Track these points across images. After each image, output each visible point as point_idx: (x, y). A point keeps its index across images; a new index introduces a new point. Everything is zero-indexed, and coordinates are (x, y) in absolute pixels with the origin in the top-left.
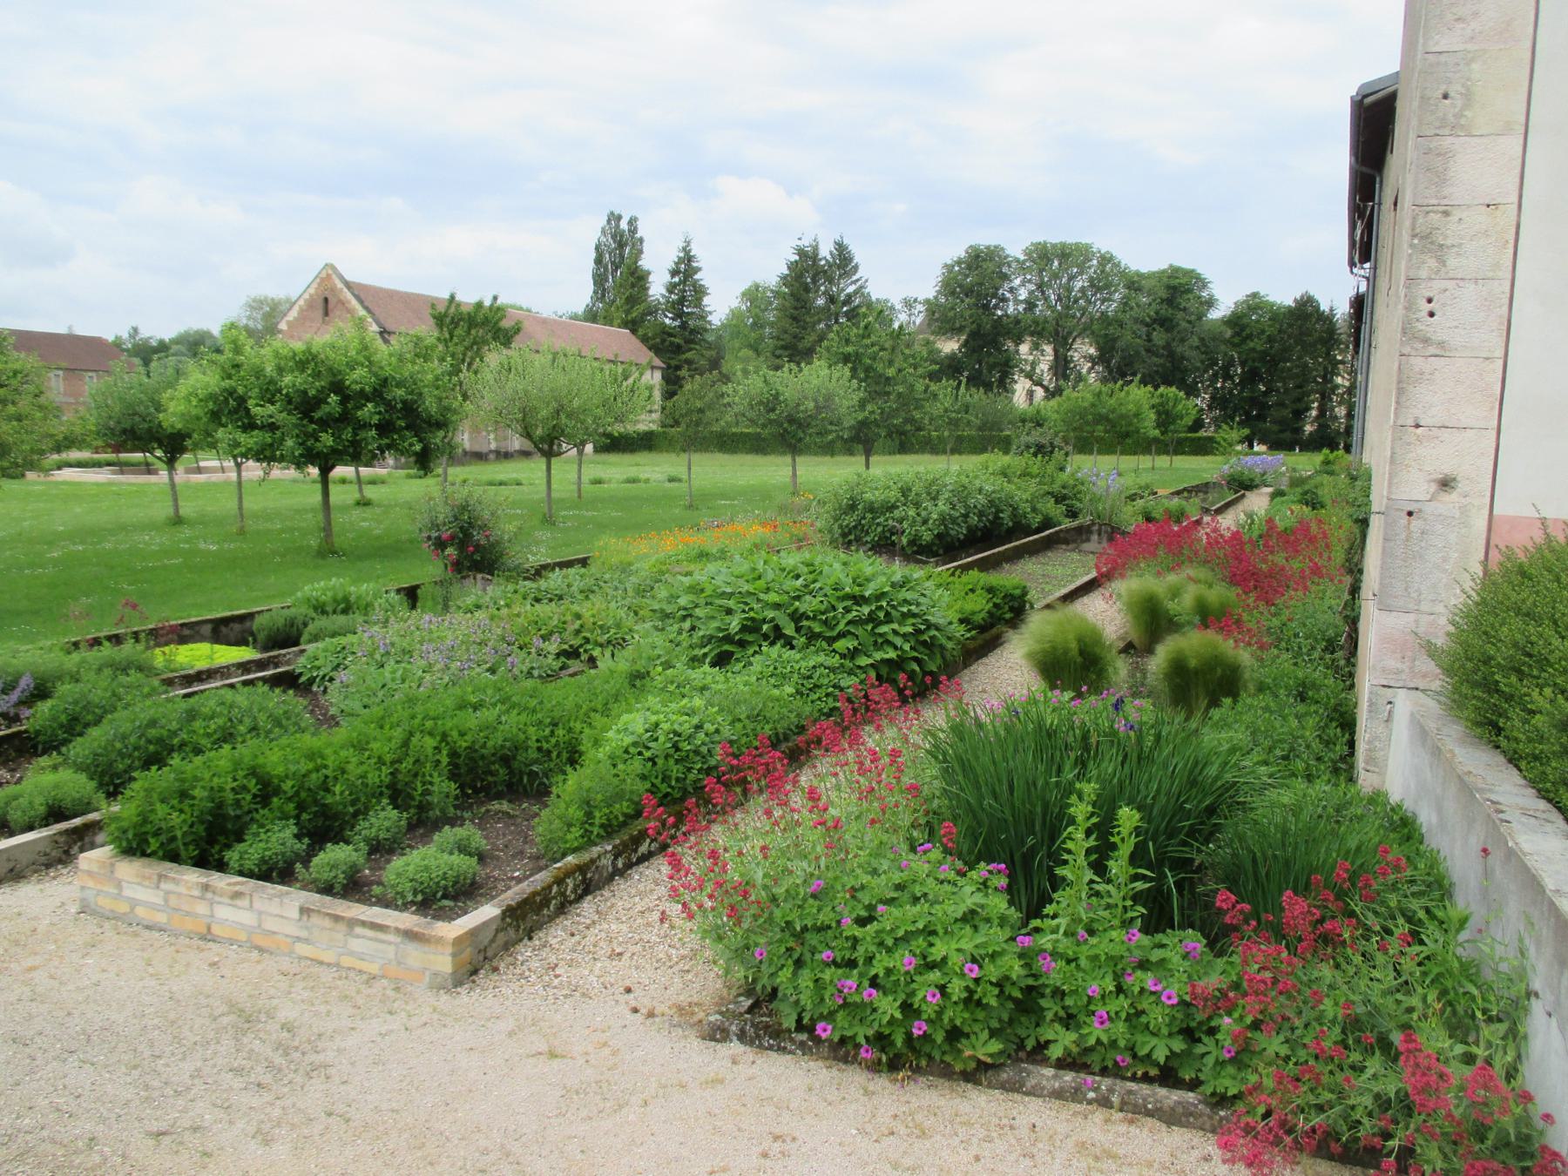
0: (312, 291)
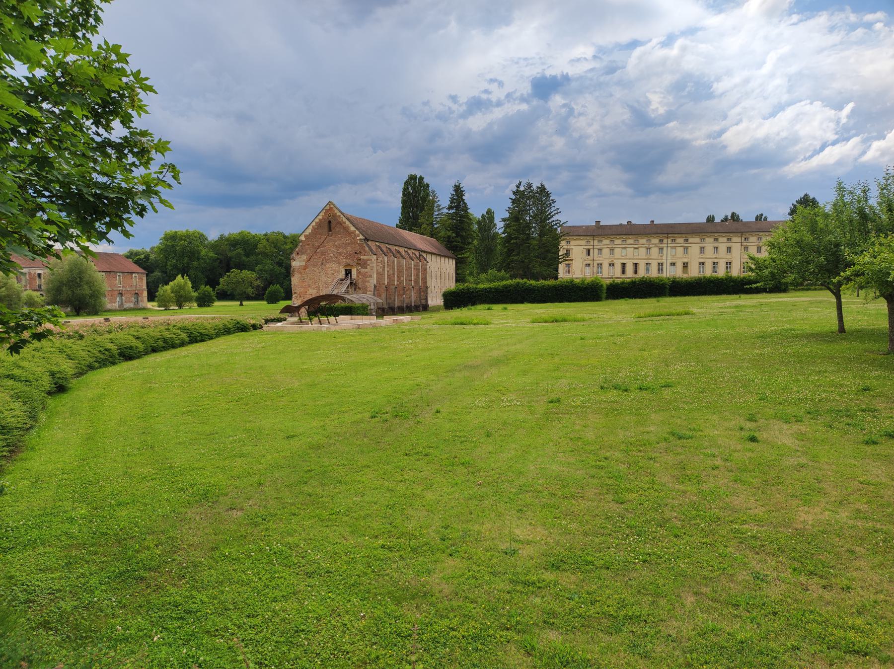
0: (320, 217)
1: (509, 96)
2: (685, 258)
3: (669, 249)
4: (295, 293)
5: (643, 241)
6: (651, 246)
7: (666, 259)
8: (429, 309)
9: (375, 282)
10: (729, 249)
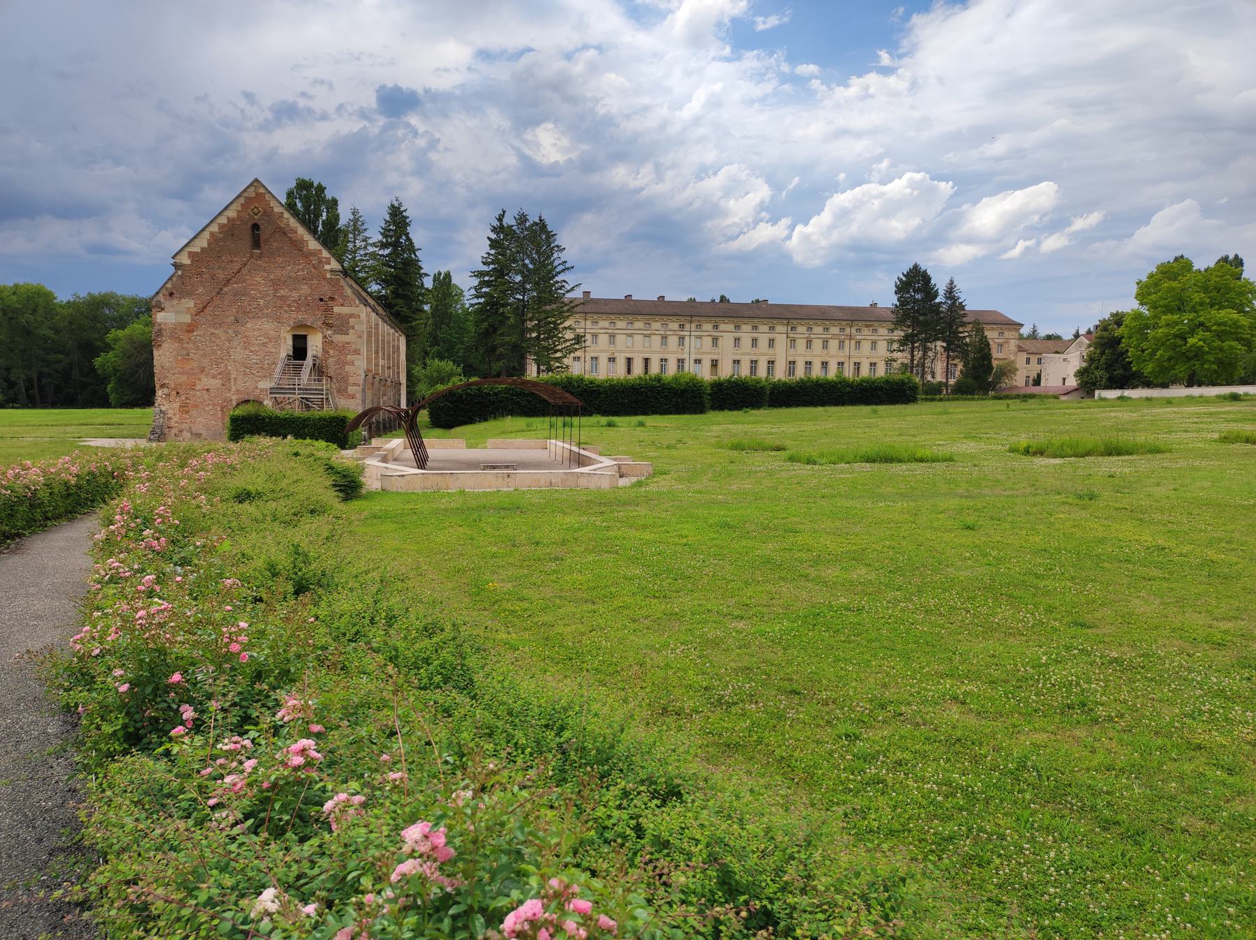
0: (232, 213)
1: (340, 108)
2: (715, 354)
3: (693, 338)
4: (163, 386)
5: (656, 325)
6: (668, 333)
7: (689, 355)
10: (771, 342)
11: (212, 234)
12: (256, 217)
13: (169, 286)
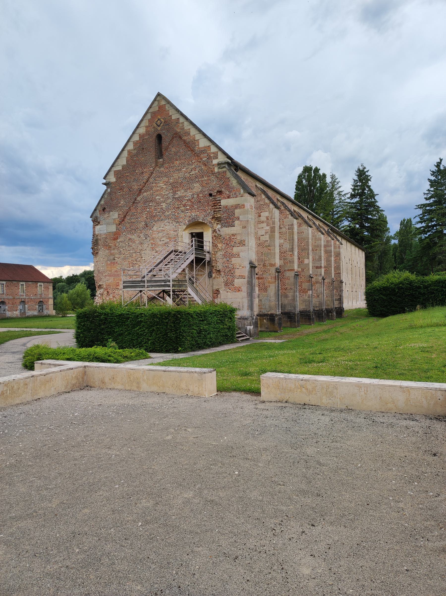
0: (142, 130)
4: (100, 287)
8: (344, 314)
9: (253, 257)
11: (129, 152)
12: (159, 128)
13: (102, 202)
